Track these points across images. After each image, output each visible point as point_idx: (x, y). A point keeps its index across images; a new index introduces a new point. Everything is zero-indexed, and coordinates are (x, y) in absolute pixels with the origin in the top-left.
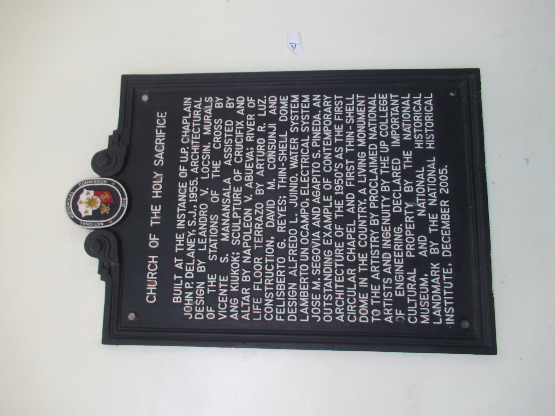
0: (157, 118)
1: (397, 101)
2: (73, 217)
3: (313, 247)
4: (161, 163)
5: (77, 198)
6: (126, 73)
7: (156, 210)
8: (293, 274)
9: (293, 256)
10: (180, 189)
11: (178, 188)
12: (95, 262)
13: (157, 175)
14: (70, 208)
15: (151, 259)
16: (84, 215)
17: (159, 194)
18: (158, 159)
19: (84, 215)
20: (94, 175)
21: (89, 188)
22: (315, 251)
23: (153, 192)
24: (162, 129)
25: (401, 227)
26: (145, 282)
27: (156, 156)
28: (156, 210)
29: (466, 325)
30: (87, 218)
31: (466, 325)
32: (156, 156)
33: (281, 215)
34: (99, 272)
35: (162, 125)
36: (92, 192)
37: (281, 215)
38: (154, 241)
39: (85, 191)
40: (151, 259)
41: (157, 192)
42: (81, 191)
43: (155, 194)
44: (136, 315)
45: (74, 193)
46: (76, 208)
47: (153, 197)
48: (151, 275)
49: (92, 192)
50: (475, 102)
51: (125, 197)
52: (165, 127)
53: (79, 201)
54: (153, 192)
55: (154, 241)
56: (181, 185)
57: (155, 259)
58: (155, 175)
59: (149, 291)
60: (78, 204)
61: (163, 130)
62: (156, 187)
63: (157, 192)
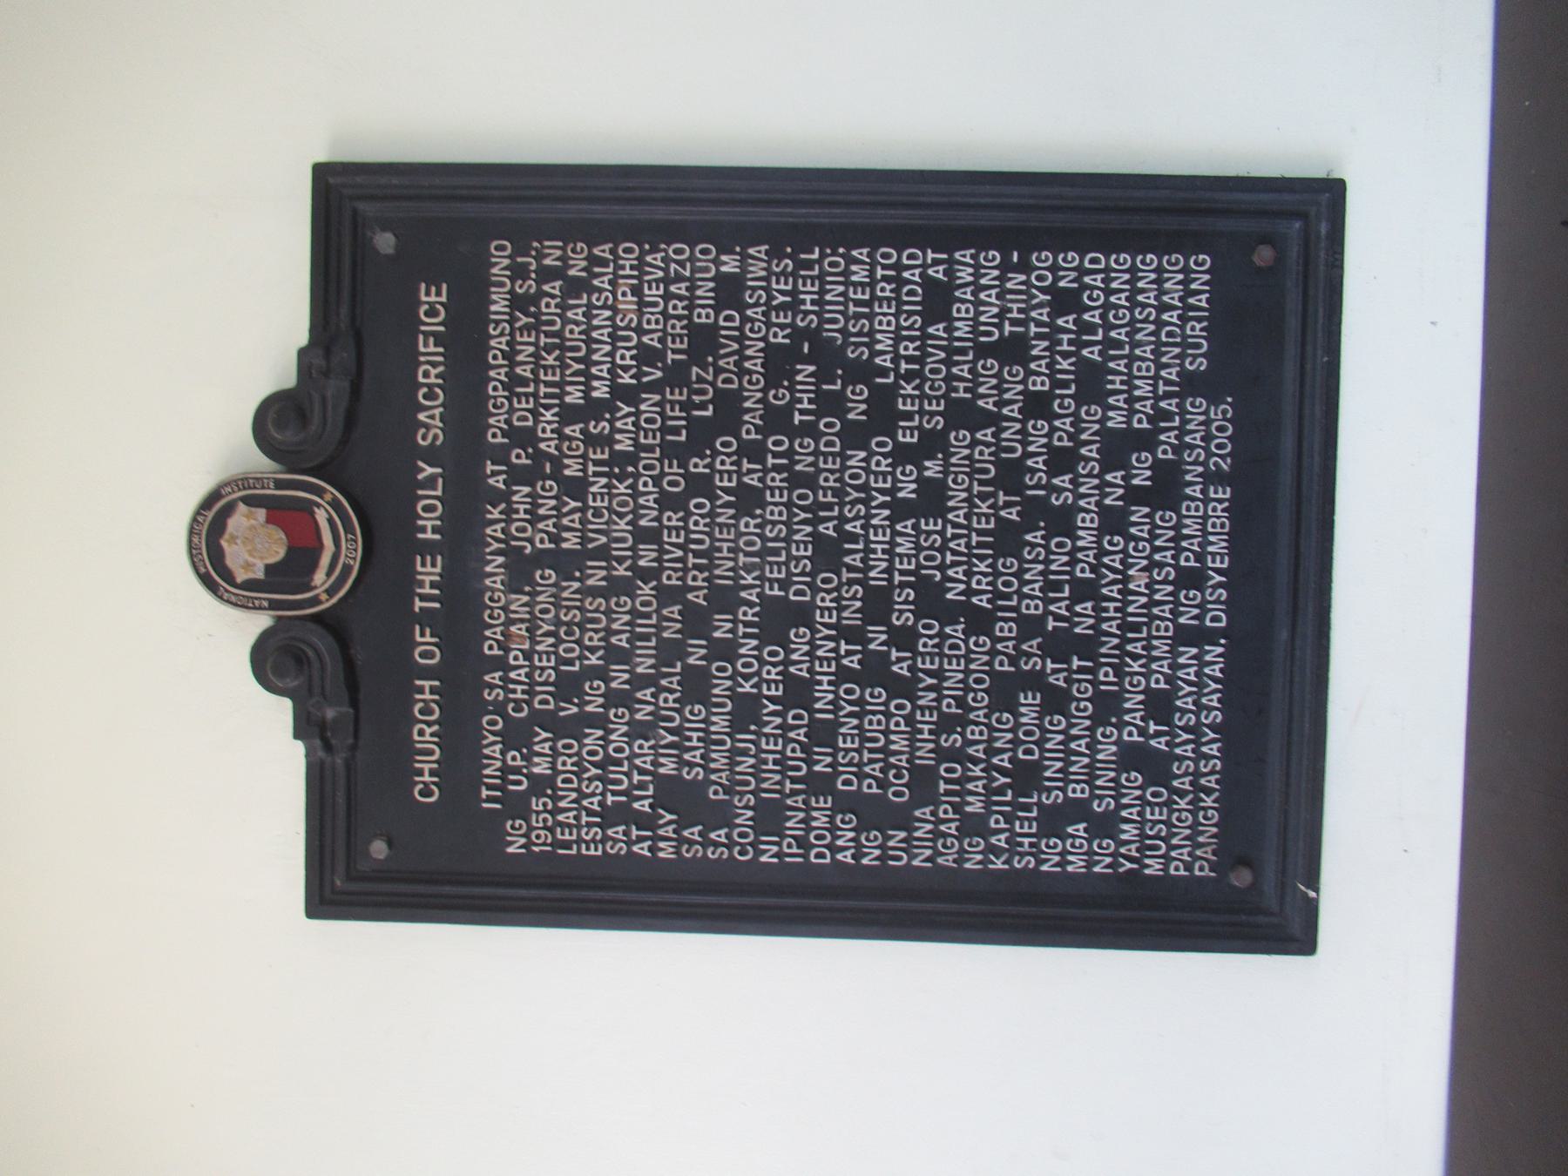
0: (421, 303)
1: (1045, 344)
2: (203, 570)
3: (929, 360)
4: (436, 437)
5: (218, 527)
6: (322, 157)
7: (429, 572)
8: (826, 531)
9: (831, 488)
10: (426, 307)
11: (420, 303)
12: (281, 710)
13: (430, 470)
14: (200, 549)
15: (421, 690)
16: (241, 577)
17: (435, 530)
18: (427, 427)
19: (241, 577)
20: (260, 463)
21: (250, 501)
22: (932, 371)
23: (420, 523)
24: (433, 334)
25: (1228, 404)
26: (408, 751)
27: (422, 417)
28: (429, 572)
29: (1241, 878)
30: (250, 585)
31: (1241, 878)
32: (422, 417)
33: (781, 299)
34: (297, 735)
35: (434, 324)
36: (261, 513)
37: (781, 299)
38: (425, 644)
39: (242, 507)
40: (421, 690)
41: (429, 526)
42: (228, 510)
43: (423, 529)
44: (390, 844)
45: (211, 515)
46: (217, 556)
47: (421, 536)
48: (425, 735)
49: (261, 513)
50: (1324, 229)
51: (325, 491)
52: (442, 328)
53: (226, 536)
54: (420, 523)
55: (425, 644)
56: (428, 294)
57: (433, 691)
58: (423, 470)
59: (420, 773)
60: (224, 544)
61: (439, 339)
62: (427, 509)
63: (429, 526)
